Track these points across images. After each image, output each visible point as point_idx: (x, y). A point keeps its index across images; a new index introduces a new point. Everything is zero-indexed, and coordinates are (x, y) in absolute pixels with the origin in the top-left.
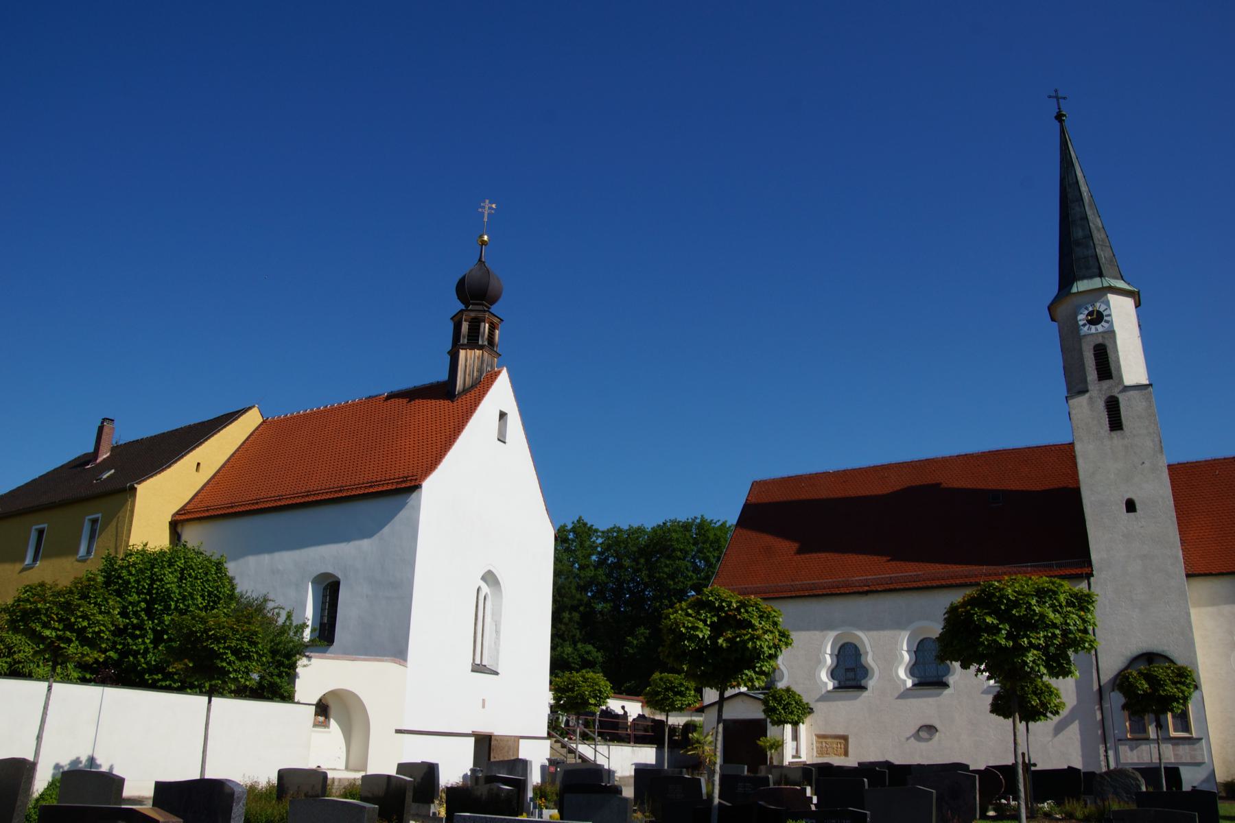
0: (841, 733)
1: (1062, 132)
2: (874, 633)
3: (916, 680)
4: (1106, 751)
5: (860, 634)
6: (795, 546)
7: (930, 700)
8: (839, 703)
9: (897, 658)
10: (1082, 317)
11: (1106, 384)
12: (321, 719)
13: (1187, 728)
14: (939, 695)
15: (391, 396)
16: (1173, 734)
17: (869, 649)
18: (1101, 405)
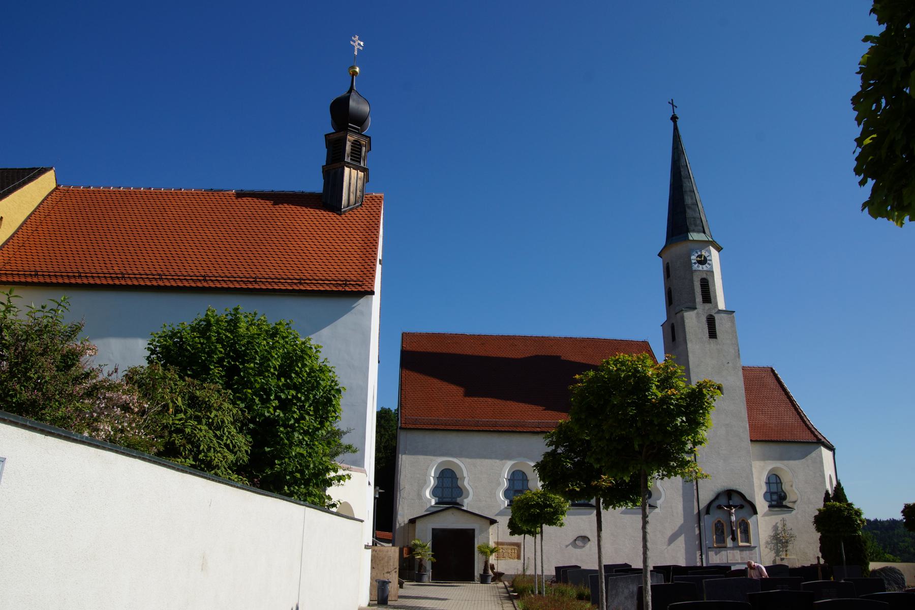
1: (676, 129)
4: (701, 555)
7: (584, 517)
9: (425, 482)
10: (694, 258)
11: (707, 306)
13: (747, 540)
15: (240, 195)
16: (741, 544)
17: (465, 474)
18: (704, 319)
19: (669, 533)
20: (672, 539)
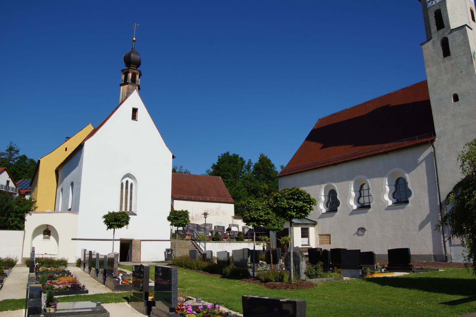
0: (327, 233)
2: (339, 183)
3: (359, 205)
5: (334, 184)
6: (321, 145)
8: (327, 219)
12: (47, 236)
14: (366, 212)
18: (439, 44)
19: (419, 222)
20: (422, 226)
